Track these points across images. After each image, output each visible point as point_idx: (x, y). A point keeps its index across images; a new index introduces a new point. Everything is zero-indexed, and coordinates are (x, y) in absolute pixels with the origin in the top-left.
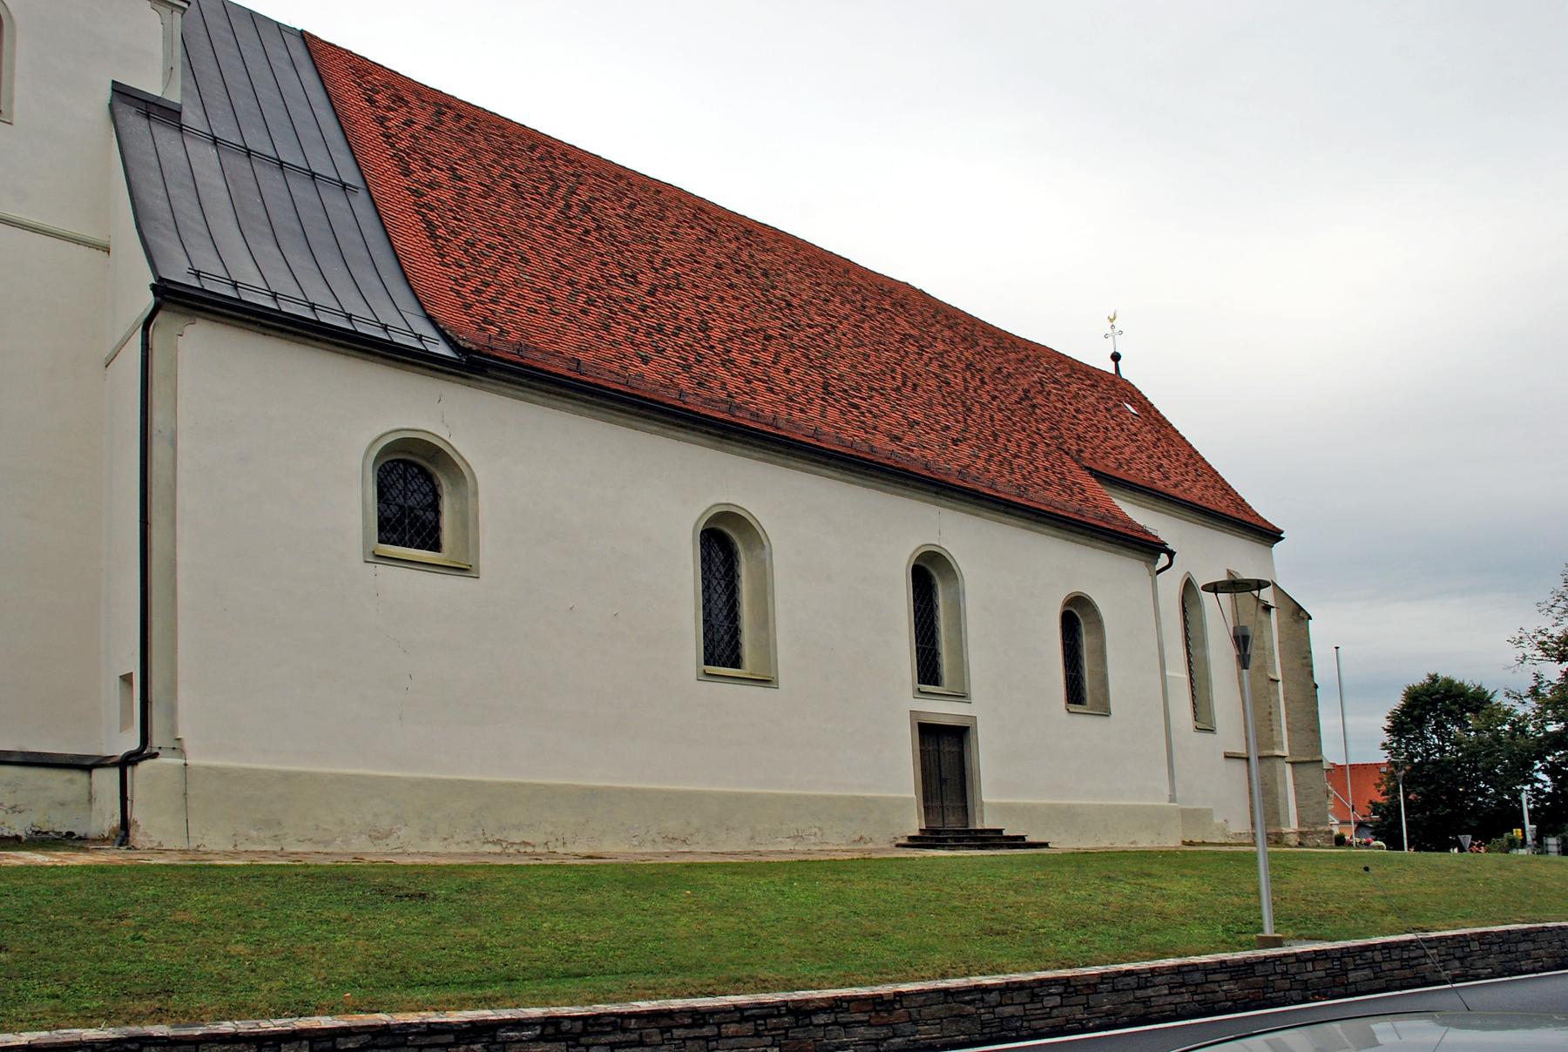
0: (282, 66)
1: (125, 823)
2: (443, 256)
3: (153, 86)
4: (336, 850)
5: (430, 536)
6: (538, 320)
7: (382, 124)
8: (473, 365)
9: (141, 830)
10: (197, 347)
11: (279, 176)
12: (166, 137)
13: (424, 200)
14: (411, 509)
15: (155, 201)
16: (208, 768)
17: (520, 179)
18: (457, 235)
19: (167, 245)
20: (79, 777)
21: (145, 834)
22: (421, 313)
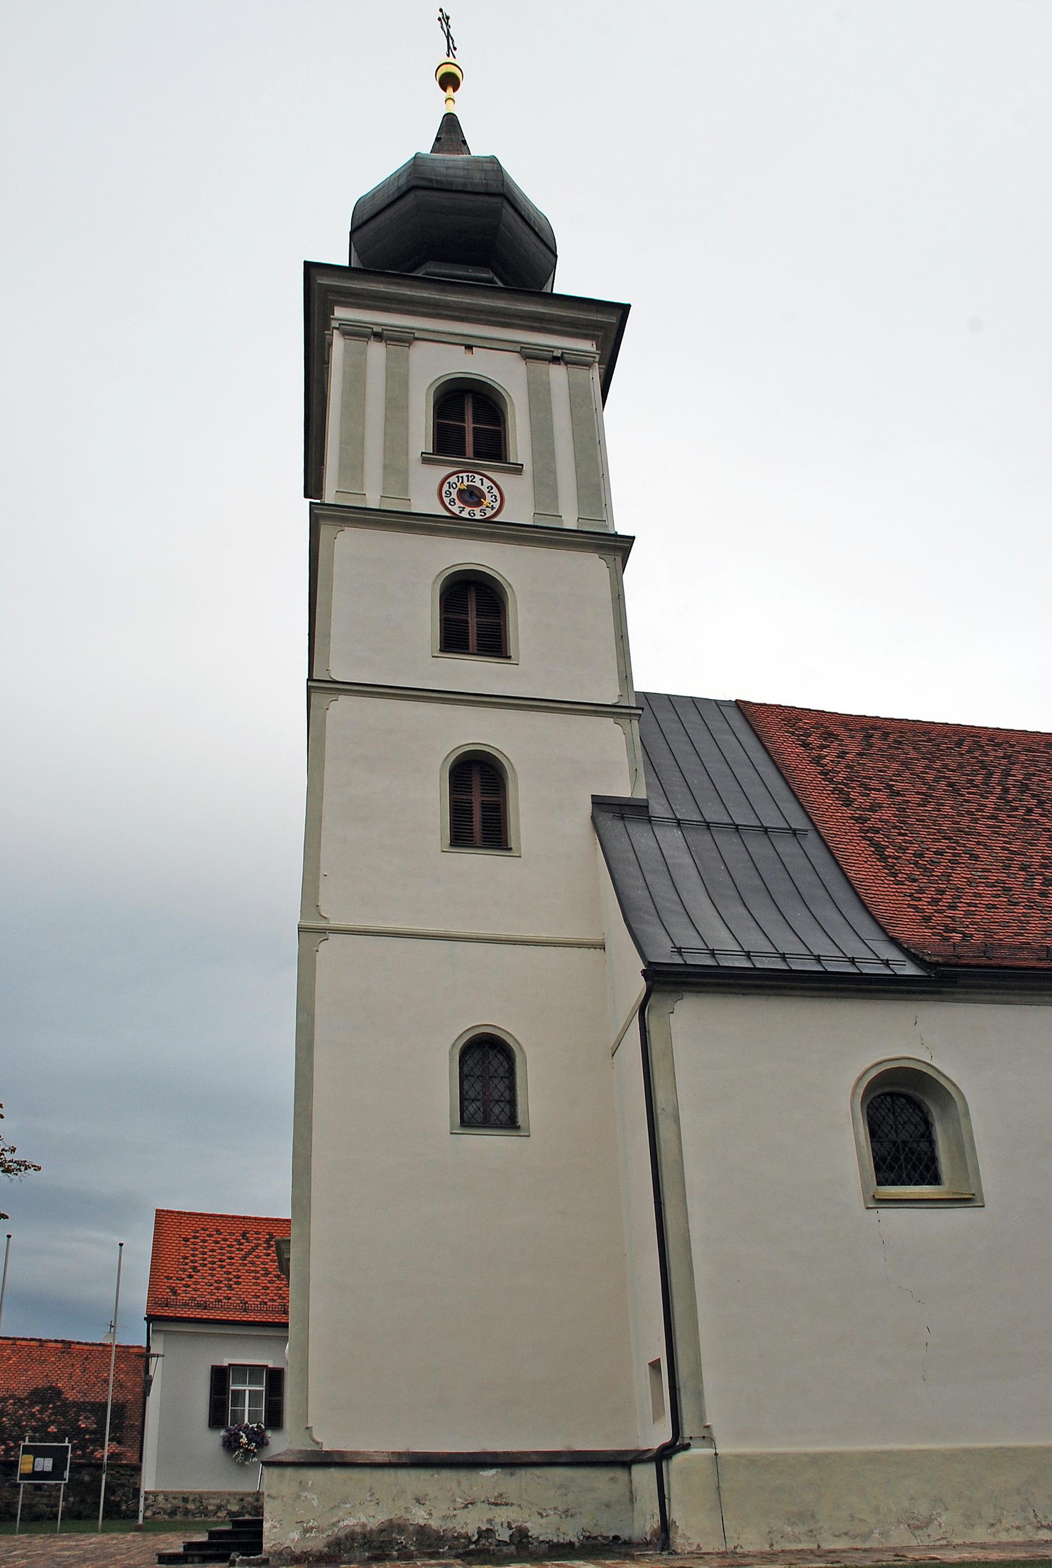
0: (726, 739)
1: (665, 1525)
2: (895, 875)
3: (622, 789)
4: (875, 1545)
5: (928, 1168)
6: (999, 915)
7: (818, 763)
8: (947, 978)
9: (680, 1532)
10: (688, 1019)
11: (736, 840)
12: (641, 834)
13: (869, 824)
14: (904, 1143)
15: (638, 893)
16: (738, 1456)
17: (954, 777)
18: (904, 850)
19: (653, 931)
20: (620, 1474)
21: (684, 1536)
22: (882, 937)
